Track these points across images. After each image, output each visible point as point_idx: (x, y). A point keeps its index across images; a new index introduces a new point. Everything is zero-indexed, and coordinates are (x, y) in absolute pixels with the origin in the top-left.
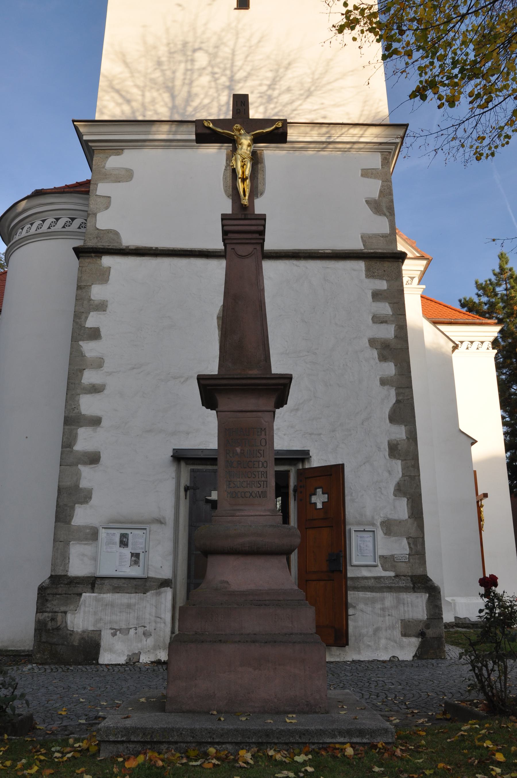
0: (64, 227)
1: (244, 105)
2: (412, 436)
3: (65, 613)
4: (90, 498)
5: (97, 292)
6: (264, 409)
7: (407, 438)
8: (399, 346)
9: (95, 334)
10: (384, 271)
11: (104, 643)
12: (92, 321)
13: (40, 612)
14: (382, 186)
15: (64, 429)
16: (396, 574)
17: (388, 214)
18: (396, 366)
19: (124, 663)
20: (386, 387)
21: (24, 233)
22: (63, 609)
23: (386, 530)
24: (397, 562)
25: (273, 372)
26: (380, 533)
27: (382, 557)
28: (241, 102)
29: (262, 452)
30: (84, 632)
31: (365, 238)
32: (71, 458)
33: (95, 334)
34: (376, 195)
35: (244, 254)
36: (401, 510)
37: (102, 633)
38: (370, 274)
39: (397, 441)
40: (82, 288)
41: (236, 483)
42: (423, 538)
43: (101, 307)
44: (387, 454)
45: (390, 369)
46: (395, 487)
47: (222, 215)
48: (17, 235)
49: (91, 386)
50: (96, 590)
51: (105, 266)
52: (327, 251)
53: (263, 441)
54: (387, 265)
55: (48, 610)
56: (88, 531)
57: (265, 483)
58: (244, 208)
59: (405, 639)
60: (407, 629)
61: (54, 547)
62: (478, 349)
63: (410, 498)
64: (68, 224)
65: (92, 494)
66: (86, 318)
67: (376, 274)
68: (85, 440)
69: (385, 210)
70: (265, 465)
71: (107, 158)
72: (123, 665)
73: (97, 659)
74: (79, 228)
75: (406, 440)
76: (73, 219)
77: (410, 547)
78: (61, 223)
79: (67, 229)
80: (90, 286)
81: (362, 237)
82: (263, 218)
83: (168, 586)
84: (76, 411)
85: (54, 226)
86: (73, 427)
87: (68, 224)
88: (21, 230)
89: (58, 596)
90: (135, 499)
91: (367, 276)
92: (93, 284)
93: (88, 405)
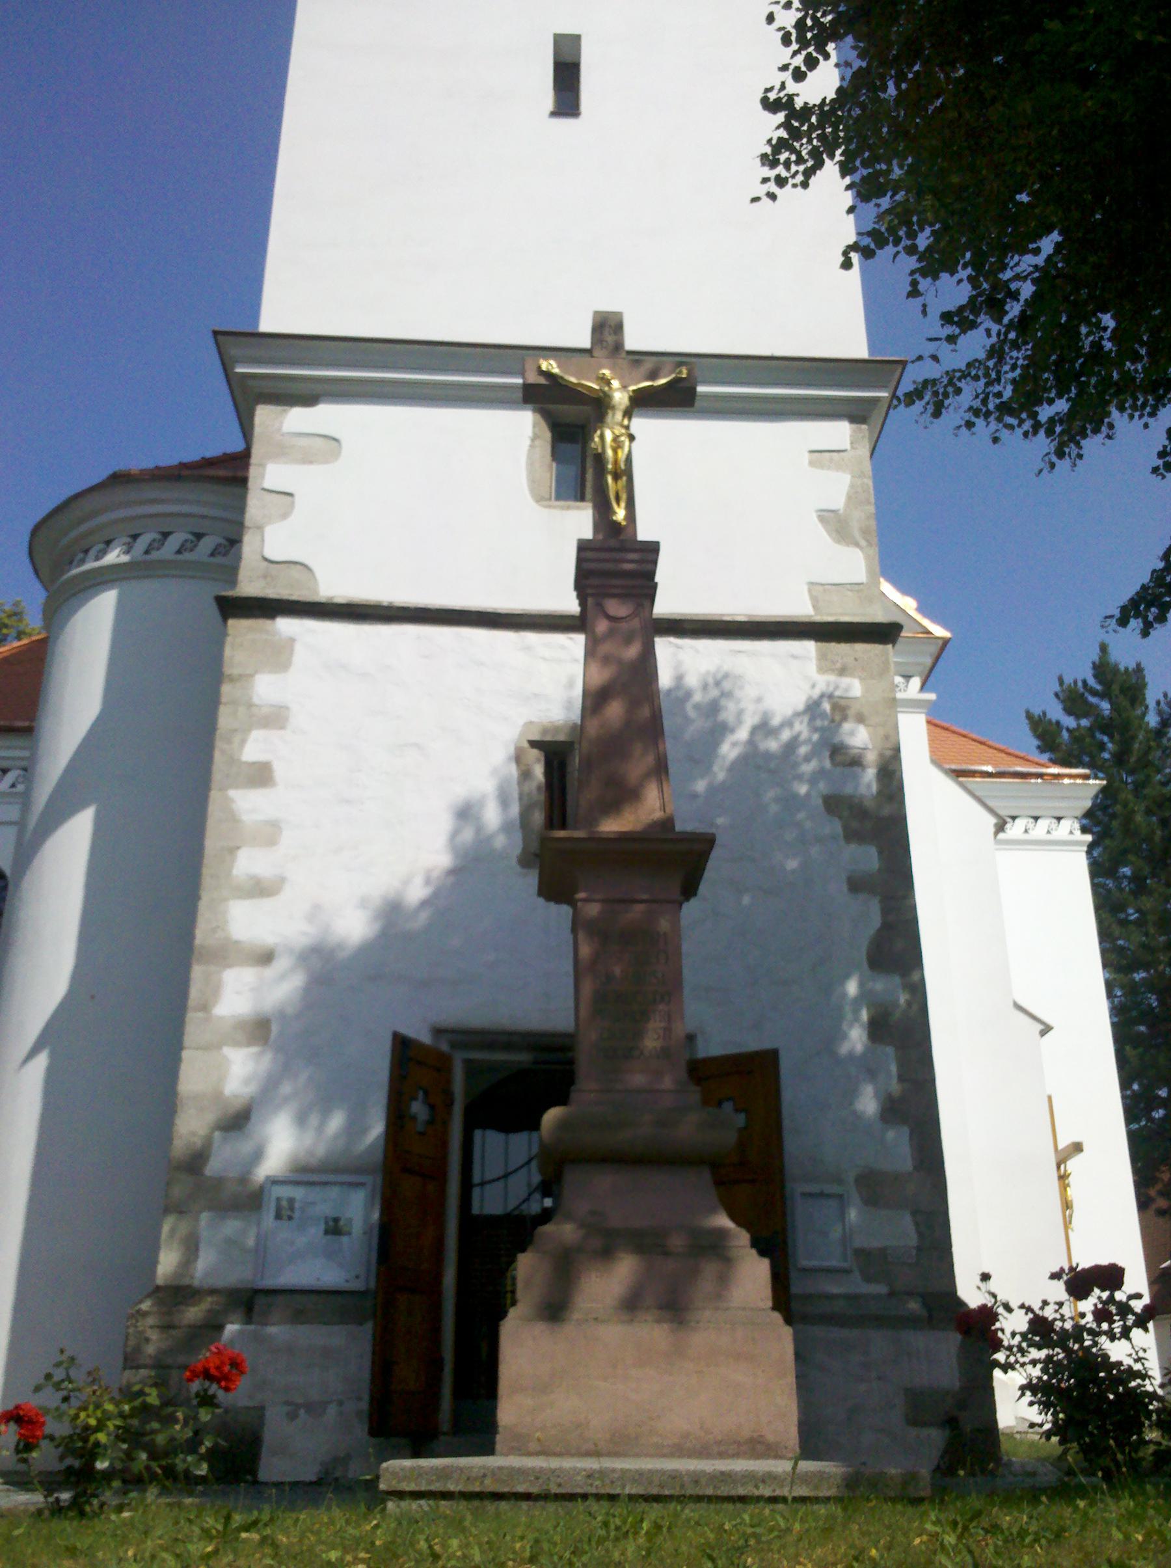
0: (179, 552)
11: (269, 1437)
13: (131, 1368)
14: (852, 486)
18: (880, 853)
19: (314, 1478)
27: (860, 1253)
31: (816, 589)
37: (268, 1414)
45: (868, 858)
58: (616, 528)
59: (913, 1432)
66: (243, 742)
72: (311, 1483)
73: (253, 1472)
76: (199, 536)
78: (207, 544)
79: (187, 556)
80: (252, 676)
82: (652, 550)
87: (189, 545)
92: (256, 672)
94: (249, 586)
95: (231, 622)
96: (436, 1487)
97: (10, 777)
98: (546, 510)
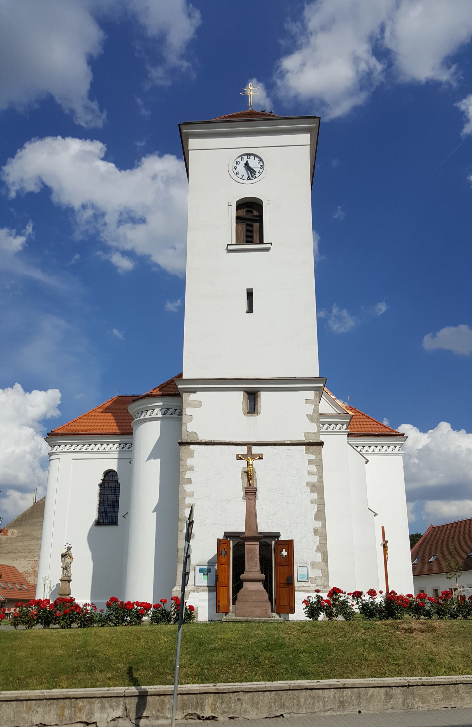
14: (314, 408)
26: (310, 568)
31: (306, 434)
34: (311, 412)
36: (319, 558)
38: (307, 452)
44: (313, 534)
45: (315, 496)
47: (225, 532)
78: (170, 412)
91: (306, 453)
94: (185, 438)
95: (181, 447)
96: (130, 695)
98: (246, 417)
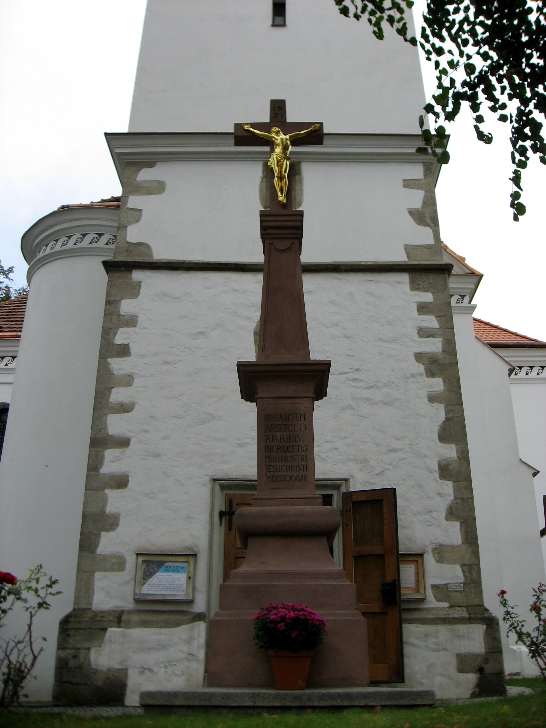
1: (281, 109)
2: (464, 456)
3: (89, 649)
4: (117, 525)
5: (127, 306)
6: (303, 395)
7: (458, 457)
8: (448, 361)
9: (124, 351)
10: (430, 283)
12: (121, 337)
15: (90, 451)
16: (450, 604)
17: (432, 225)
18: (444, 382)
20: (435, 405)
21: (48, 251)
22: (87, 645)
23: (439, 557)
24: (451, 592)
25: (312, 358)
28: (278, 108)
29: (301, 437)
30: (109, 670)
32: (98, 482)
33: (124, 351)
35: (282, 249)
36: (453, 534)
38: (414, 287)
39: (448, 461)
40: (111, 303)
41: (275, 467)
42: (478, 565)
43: (131, 322)
45: (438, 384)
46: (447, 510)
48: (42, 251)
49: (119, 405)
50: (122, 624)
51: (135, 280)
52: (369, 264)
53: (303, 426)
54: (432, 278)
55: (70, 646)
56: (114, 560)
57: (305, 467)
60: (464, 663)
61: (77, 578)
62: (538, 374)
63: (463, 522)
64: (95, 240)
65: (119, 521)
66: (115, 334)
67: (421, 286)
68: (112, 462)
69: (428, 220)
70: (305, 449)
71: (139, 170)
74: (107, 244)
75: (458, 461)
76: (100, 235)
77: (465, 576)
79: (94, 245)
80: (120, 301)
81: (405, 249)
83: (200, 620)
84: (103, 431)
85: (81, 242)
86: (99, 449)
88: (45, 247)
89: (81, 631)
90: (171, 500)
92: (122, 299)
93: (115, 425)
97: (5, 361)
